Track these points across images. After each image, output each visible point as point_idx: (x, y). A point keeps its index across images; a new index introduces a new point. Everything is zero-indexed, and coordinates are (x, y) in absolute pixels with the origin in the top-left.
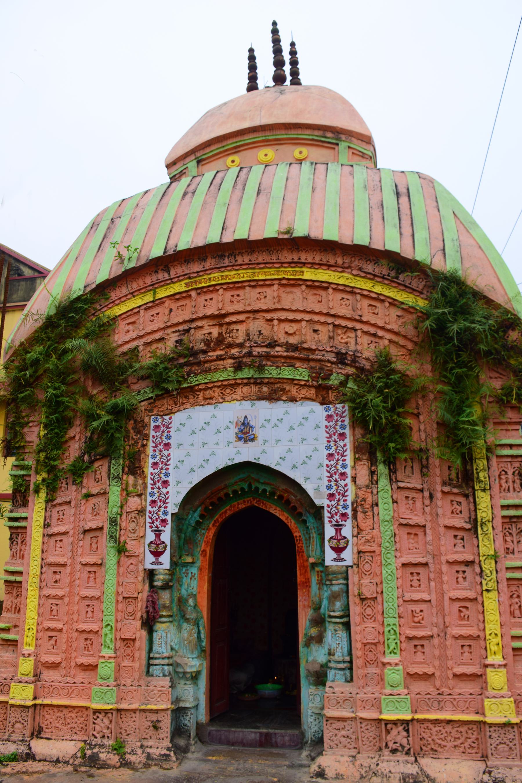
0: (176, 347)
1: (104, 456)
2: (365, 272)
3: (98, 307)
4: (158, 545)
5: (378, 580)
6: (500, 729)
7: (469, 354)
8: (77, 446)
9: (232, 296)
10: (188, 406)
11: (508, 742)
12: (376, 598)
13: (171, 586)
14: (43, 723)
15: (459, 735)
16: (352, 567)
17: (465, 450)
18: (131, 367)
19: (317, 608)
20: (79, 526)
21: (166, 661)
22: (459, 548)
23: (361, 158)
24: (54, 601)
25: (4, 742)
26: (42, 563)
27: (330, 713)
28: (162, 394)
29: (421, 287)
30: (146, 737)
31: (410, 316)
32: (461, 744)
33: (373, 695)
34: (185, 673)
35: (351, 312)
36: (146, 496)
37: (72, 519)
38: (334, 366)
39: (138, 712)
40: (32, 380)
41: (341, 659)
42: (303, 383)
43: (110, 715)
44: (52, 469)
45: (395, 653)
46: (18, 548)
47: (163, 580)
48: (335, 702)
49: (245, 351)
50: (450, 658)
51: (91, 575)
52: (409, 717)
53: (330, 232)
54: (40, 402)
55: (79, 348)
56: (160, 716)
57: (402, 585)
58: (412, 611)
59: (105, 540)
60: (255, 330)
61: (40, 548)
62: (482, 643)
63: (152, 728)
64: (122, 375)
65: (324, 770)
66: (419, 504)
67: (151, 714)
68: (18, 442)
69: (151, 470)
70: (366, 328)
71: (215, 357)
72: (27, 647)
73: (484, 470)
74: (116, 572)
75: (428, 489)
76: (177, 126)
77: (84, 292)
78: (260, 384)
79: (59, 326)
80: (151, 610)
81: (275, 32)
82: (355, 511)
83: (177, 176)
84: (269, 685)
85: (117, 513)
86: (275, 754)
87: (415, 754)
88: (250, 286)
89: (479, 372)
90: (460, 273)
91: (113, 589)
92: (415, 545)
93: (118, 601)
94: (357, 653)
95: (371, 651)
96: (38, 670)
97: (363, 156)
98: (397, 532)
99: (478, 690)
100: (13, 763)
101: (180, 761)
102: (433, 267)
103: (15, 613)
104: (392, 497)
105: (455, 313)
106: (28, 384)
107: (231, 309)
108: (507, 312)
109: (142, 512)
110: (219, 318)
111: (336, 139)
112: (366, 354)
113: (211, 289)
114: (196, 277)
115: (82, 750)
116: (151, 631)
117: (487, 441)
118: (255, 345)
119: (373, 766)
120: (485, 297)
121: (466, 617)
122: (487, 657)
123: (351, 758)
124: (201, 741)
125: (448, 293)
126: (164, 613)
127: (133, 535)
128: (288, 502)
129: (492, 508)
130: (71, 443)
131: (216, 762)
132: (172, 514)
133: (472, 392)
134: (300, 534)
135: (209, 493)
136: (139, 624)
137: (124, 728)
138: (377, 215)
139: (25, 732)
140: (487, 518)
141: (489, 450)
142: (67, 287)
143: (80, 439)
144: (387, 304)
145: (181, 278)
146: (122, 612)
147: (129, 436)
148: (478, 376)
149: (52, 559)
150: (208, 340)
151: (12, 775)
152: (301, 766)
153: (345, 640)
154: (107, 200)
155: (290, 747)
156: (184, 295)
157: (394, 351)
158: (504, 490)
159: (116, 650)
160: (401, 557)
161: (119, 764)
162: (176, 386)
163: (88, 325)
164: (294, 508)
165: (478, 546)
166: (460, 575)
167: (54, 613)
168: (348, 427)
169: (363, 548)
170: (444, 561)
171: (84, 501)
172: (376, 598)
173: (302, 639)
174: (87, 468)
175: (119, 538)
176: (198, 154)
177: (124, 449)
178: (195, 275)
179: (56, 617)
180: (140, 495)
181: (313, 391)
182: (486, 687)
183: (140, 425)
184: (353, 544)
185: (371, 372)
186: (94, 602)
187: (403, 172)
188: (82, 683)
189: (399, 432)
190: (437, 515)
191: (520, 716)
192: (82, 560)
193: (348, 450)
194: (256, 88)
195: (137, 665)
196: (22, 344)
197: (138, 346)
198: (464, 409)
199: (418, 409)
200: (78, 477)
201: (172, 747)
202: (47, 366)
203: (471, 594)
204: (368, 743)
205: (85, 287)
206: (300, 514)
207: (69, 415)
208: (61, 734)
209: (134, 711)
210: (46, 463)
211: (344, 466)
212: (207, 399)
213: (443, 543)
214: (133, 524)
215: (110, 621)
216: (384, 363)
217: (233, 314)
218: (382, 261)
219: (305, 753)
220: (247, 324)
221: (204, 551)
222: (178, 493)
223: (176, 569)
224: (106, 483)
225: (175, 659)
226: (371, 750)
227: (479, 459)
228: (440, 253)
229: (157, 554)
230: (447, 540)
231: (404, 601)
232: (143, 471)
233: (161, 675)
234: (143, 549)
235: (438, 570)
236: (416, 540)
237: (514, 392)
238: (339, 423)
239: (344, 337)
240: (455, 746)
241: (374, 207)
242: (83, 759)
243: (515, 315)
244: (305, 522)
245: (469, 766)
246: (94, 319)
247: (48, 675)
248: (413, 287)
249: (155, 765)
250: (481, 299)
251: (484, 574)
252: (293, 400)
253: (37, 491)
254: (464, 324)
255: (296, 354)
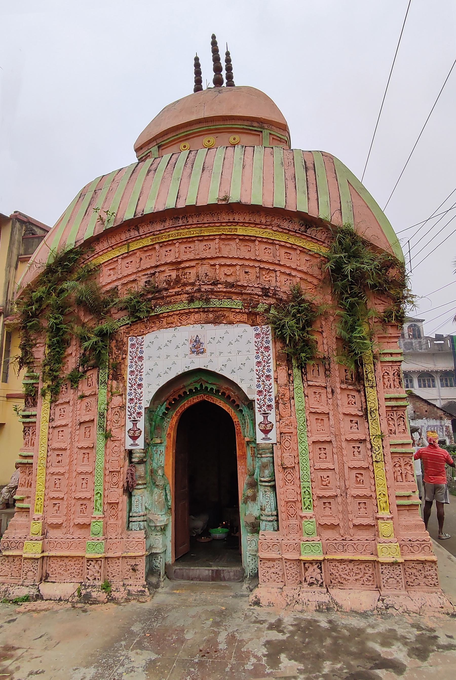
0: (146, 286)
1: (94, 367)
2: (282, 228)
7: (360, 287)
8: (74, 360)
9: (186, 248)
10: (156, 329)
11: (396, 577)
12: (294, 467)
14: (49, 570)
15: (359, 571)
16: (276, 444)
17: (357, 358)
18: (112, 301)
20: (76, 419)
21: (142, 518)
23: (279, 142)
25: (19, 587)
26: (48, 448)
27: (262, 555)
28: (136, 321)
30: (127, 577)
31: (315, 260)
32: (360, 578)
33: (294, 541)
34: (156, 527)
35: (273, 258)
37: (71, 414)
38: (260, 298)
40: (38, 313)
41: (270, 513)
42: (238, 311)
43: (99, 562)
44: (55, 378)
45: (310, 509)
46: (30, 438)
48: (266, 546)
49: (196, 288)
51: (85, 456)
52: (321, 558)
53: (256, 199)
54: (45, 329)
55: (73, 288)
56: (137, 561)
57: (313, 457)
62: (374, 501)
63: (131, 570)
64: (106, 307)
66: (324, 397)
68: (28, 359)
69: (129, 376)
70: (283, 270)
72: (37, 513)
74: (104, 453)
75: (331, 386)
76: (141, 119)
77: (75, 246)
78: (207, 312)
79: (57, 271)
80: (130, 480)
81: (214, 43)
83: (144, 158)
85: (104, 409)
87: (327, 586)
88: (198, 240)
89: (367, 300)
90: (353, 226)
91: (102, 465)
93: (105, 474)
95: (291, 507)
96: (46, 530)
97: (280, 140)
100: (26, 603)
101: (153, 595)
103: (27, 487)
104: (304, 392)
105: (349, 257)
106: (35, 315)
108: (389, 255)
110: (176, 264)
112: (284, 289)
113: (170, 243)
114: (158, 234)
115: (79, 590)
116: (130, 496)
118: (203, 283)
120: (372, 244)
121: (361, 481)
122: (378, 512)
125: (343, 242)
126: (140, 482)
127: (116, 425)
128: (229, 397)
130: (69, 358)
131: (179, 595)
134: (238, 420)
135: (171, 392)
137: (110, 571)
138: (291, 185)
139: (35, 578)
140: (375, 408)
141: (375, 357)
142: (62, 242)
143: (76, 355)
145: (147, 235)
146: (109, 482)
147: (112, 352)
148: (366, 303)
149: (55, 445)
150: (169, 281)
151: (24, 613)
152: (243, 596)
153: (273, 499)
154: (92, 176)
156: (150, 248)
157: (303, 286)
158: (387, 387)
159: (104, 512)
161: (107, 599)
162: (146, 314)
165: (368, 428)
166: (356, 450)
167: (58, 485)
168: (271, 342)
169: (284, 430)
171: (80, 401)
172: (294, 467)
173: (241, 499)
175: (106, 427)
178: (158, 232)
179: (58, 489)
180: (121, 395)
181: (245, 316)
183: (120, 344)
185: (287, 302)
186: (88, 476)
187: (310, 152)
188: (79, 538)
189: (308, 345)
190: (337, 405)
193: (272, 359)
194: (201, 89)
195: (119, 522)
196: (29, 285)
197: (118, 286)
199: (322, 328)
200: (75, 383)
201: (147, 584)
202: (49, 302)
203: (365, 465)
205: (76, 242)
206: (238, 406)
208: (63, 578)
209: (118, 558)
210: (50, 374)
211: (269, 371)
212: (169, 323)
213: (342, 426)
215: (100, 490)
216: (297, 295)
218: (294, 219)
219: (245, 586)
220: (197, 269)
222: (149, 392)
228: (338, 212)
229: (134, 438)
230: (345, 424)
231: (315, 469)
232: (123, 377)
233: (138, 529)
234: (124, 435)
237: (394, 314)
238: (265, 339)
242: (79, 597)
244: (241, 411)
245: (367, 595)
246: (84, 266)
247: (52, 533)
249: (134, 599)
250: (368, 246)
251: (373, 449)
252: (231, 323)
253: (44, 395)
255: (233, 290)
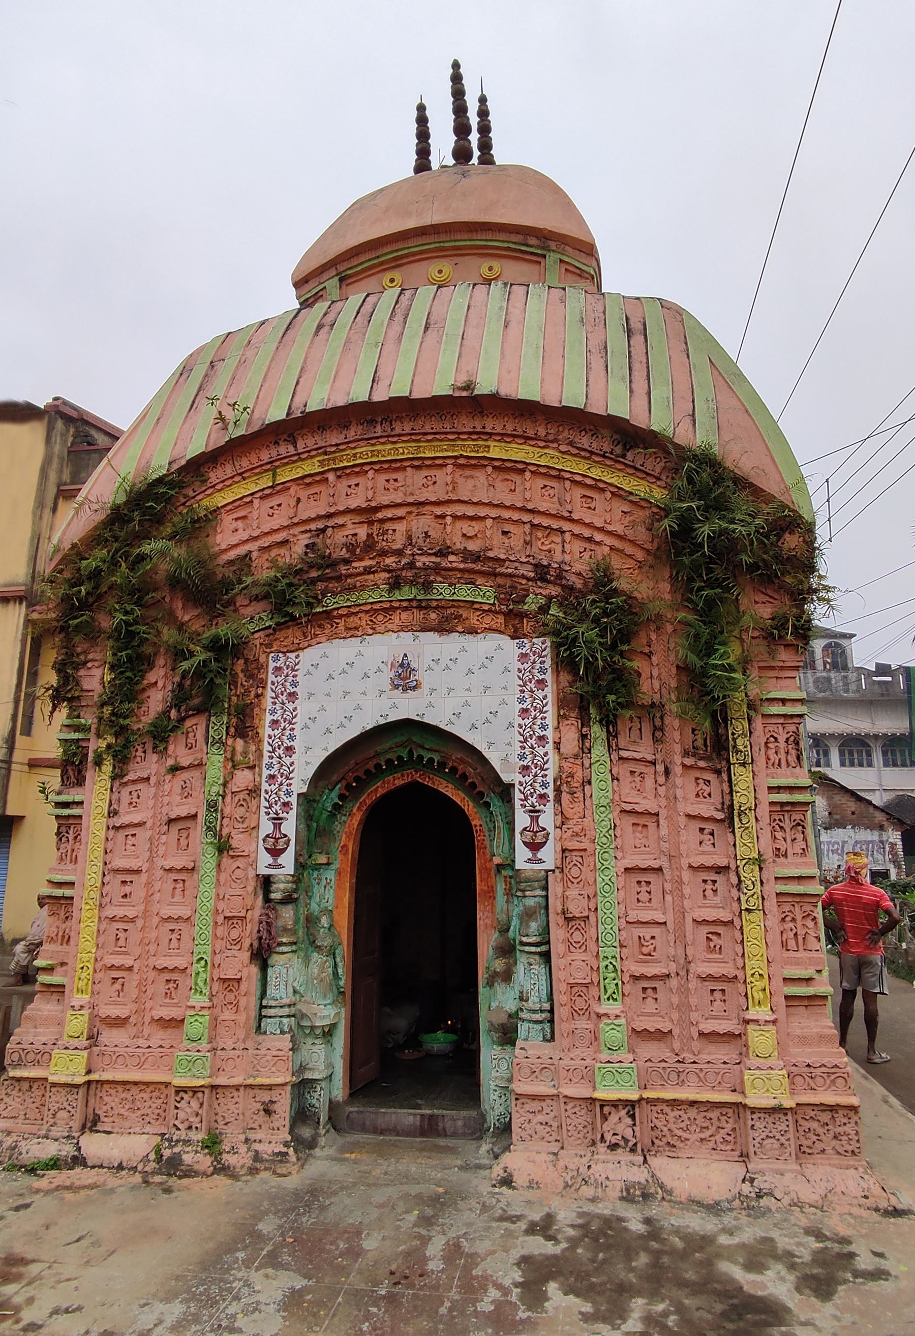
0: (306, 553)
1: (199, 711)
2: (578, 448)
3: (191, 494)
4: (277, 839)
5: (590, 891)
6: (767, 1116)
7: (725, 569)
8: (160, 696)
9: (388, 481)
10: (323, 639)
11: (778, 1136)
12: (588, 917)
13: (297, 899)
14: (100, 1109)
16: (553, 871)
18: (240, 582)
19: (504, 930)
20: (161, 813)
21: (286, 1011)
22: (707, 847)
23: (578, 278)
24: (121, 926)
25: (40, 1140)
27: (520, 1087)
28: (286, 622)
29: (658, 470)
30: (253, 1126)
34: (313, 1028)
35: (557, 506)
36: (261, 768)
37: (151, 803)
38: (530, 583)
39: (242, 1089)
40: (91, 600)
41: (537, 1007)
43: (200, 1095)
45: (615, 1000)
47: (283, 891)
48: (528, 1072)
49: (405, 561)
50: (694, 1008)
51: (178, 886)
52: (635, 1097)
53: (528, 387)
55: (163, 554)
56: (274, 1095)
57: (625, 899)
58: (640, 937)
59: (198, 832)
60: (420, 530)
61: (102, 846)
62: (741, 988)
63: (262, 1113)
65: (511, 1176)
66: (649, 782)
67: (261, 1091)
69: (268, 731)
70: (577, 530)
71: (361, 569)
72: (79, 996)
73: (743, 735)
74: (214, 880)
75: (663, 761)
76: (307, 225)
77: (168, 470)
78: (425, 608)
79: (131, 520)
81: (457, 78)
82: (558, 791)
83: (310, 301)
84: (440, 1035)
86: (441, 1147)
87: (644, 1151)
88: (412, 467)
89: (739, 594)
90: (716, 449)
91: (210, 905)
92: (643, 841)
94: (560, 998)
95: (579, 995)
96: (96, 1030)
97: (581, 274)
98: (618, 822)
99: (734, 1056)
100: (53, 1172)
101: (302, 1162)
102: (676, 440)
104: (611, 771)
106: (85, 605)
107: (385, 500)
108: (784, 506)
109: (255, 791)
110: (368, 513)
111: (545, 247)
114: (334, 452)
115: (158, 1151)
116: (264, 967)
117: (749, 694)
118: (419, 552)
119: (583, 1170)
120: (752, 485)
122: (747, 1008)
123: (551, 1157)
124: (335, 1129)
125: (696, 478)
126: (284, 940)
127: (241, 826)
128: (464, 777)
129: (755, 790)
131: (355, 1162)
132: (299, 795)
133: (727, 623)
135: (351, 765)
136: (246, 955)
139: (71, 1124)
141: (751, 706)
142: (144, 462)
143: (164, 687)
144: (609, 495)
146: (222, 939)
148: (737, 599)
149: (119, 862)
150: (353, 545)
151: (48, 1192)
152: (479, 1167)
155: (464, 1135)
156: (317, 478)
157: (616, 563)
160: (623, 858)
162: (306, 610)
163: (176, 519)
164: (473, 785)
165: (735, 845)
166: (709, 886)
167: (121, 942)
168: (549, 670)
169: (573, 844)
170: (685, 866)
172: (588, 917)
174: (174, 729)
175: (221, 830)
176: (341, 268)
177: (230, 699)
178: (334, 449)
179: (123, 949)
180: (252, 768)
181: (501, 619)
182: (748, 1053)
183: (253, 666)
184: (555, 839)
187: (638, 299)
188: (161, 1046)
189: (623, 680)
190: (675, 798)
191: (795, 1096)
192: (165, 863)
193: (550, 704)
196: (74, 546)
197: (251, 552)
198: (717, 647)
199: (650, 646)
202: (113, 579)
203: (725, 916)
204: (575, 1133)
205: (170, 463)
206: (481, 794)
207: (148, 651)
208: (127, 1124)
209: (237, 1088)
210: (113, 722)
211: (543, 727)
212: (350, 629)
213: (683, 839)
214: (242, 808)
215: (204, 952)
216: (602, 580)
217: (388, 507)
219: (485, 1147)
220: (409, 523)
221: (345, 846)
222: (307, 763)
223: (303, 874)
224: (202, 750)
225: (298, 1007)
226: (580, 1145)
227: (736, 719)
228: (688, 420)
229: (275, 852)
230: (690, 835)
231: (627, 922)
232: (257, 733)
233: (278, 1032)
234: (255, 846)
235: (676, 878)
236: (645, 834)
238: (538, 666)
239: (546, 543)
240: (702, 1140)
241: (594, 351)
242: (158, 1163)
243: (794, 511)
244: (487, 805)
246: (185, 511)
247: (109, 1037)
248: (647, 470)
249: (266, 1169)
251: (743, 885)
252: (473, 631)
253: (98, 763)
254: (719, 524)
255: (478, 567)
